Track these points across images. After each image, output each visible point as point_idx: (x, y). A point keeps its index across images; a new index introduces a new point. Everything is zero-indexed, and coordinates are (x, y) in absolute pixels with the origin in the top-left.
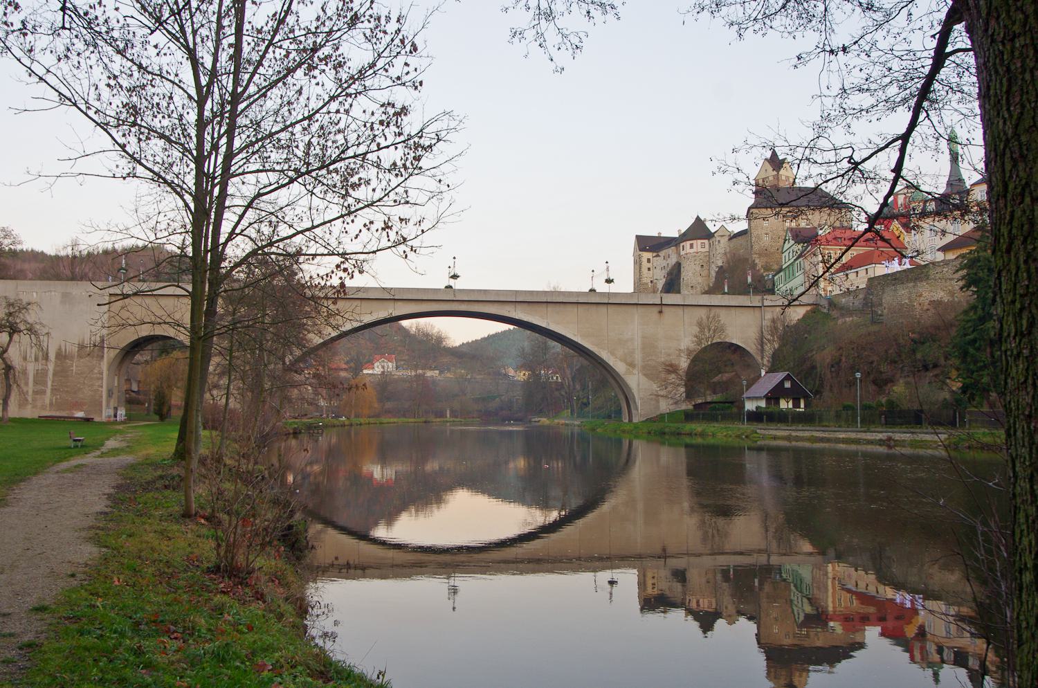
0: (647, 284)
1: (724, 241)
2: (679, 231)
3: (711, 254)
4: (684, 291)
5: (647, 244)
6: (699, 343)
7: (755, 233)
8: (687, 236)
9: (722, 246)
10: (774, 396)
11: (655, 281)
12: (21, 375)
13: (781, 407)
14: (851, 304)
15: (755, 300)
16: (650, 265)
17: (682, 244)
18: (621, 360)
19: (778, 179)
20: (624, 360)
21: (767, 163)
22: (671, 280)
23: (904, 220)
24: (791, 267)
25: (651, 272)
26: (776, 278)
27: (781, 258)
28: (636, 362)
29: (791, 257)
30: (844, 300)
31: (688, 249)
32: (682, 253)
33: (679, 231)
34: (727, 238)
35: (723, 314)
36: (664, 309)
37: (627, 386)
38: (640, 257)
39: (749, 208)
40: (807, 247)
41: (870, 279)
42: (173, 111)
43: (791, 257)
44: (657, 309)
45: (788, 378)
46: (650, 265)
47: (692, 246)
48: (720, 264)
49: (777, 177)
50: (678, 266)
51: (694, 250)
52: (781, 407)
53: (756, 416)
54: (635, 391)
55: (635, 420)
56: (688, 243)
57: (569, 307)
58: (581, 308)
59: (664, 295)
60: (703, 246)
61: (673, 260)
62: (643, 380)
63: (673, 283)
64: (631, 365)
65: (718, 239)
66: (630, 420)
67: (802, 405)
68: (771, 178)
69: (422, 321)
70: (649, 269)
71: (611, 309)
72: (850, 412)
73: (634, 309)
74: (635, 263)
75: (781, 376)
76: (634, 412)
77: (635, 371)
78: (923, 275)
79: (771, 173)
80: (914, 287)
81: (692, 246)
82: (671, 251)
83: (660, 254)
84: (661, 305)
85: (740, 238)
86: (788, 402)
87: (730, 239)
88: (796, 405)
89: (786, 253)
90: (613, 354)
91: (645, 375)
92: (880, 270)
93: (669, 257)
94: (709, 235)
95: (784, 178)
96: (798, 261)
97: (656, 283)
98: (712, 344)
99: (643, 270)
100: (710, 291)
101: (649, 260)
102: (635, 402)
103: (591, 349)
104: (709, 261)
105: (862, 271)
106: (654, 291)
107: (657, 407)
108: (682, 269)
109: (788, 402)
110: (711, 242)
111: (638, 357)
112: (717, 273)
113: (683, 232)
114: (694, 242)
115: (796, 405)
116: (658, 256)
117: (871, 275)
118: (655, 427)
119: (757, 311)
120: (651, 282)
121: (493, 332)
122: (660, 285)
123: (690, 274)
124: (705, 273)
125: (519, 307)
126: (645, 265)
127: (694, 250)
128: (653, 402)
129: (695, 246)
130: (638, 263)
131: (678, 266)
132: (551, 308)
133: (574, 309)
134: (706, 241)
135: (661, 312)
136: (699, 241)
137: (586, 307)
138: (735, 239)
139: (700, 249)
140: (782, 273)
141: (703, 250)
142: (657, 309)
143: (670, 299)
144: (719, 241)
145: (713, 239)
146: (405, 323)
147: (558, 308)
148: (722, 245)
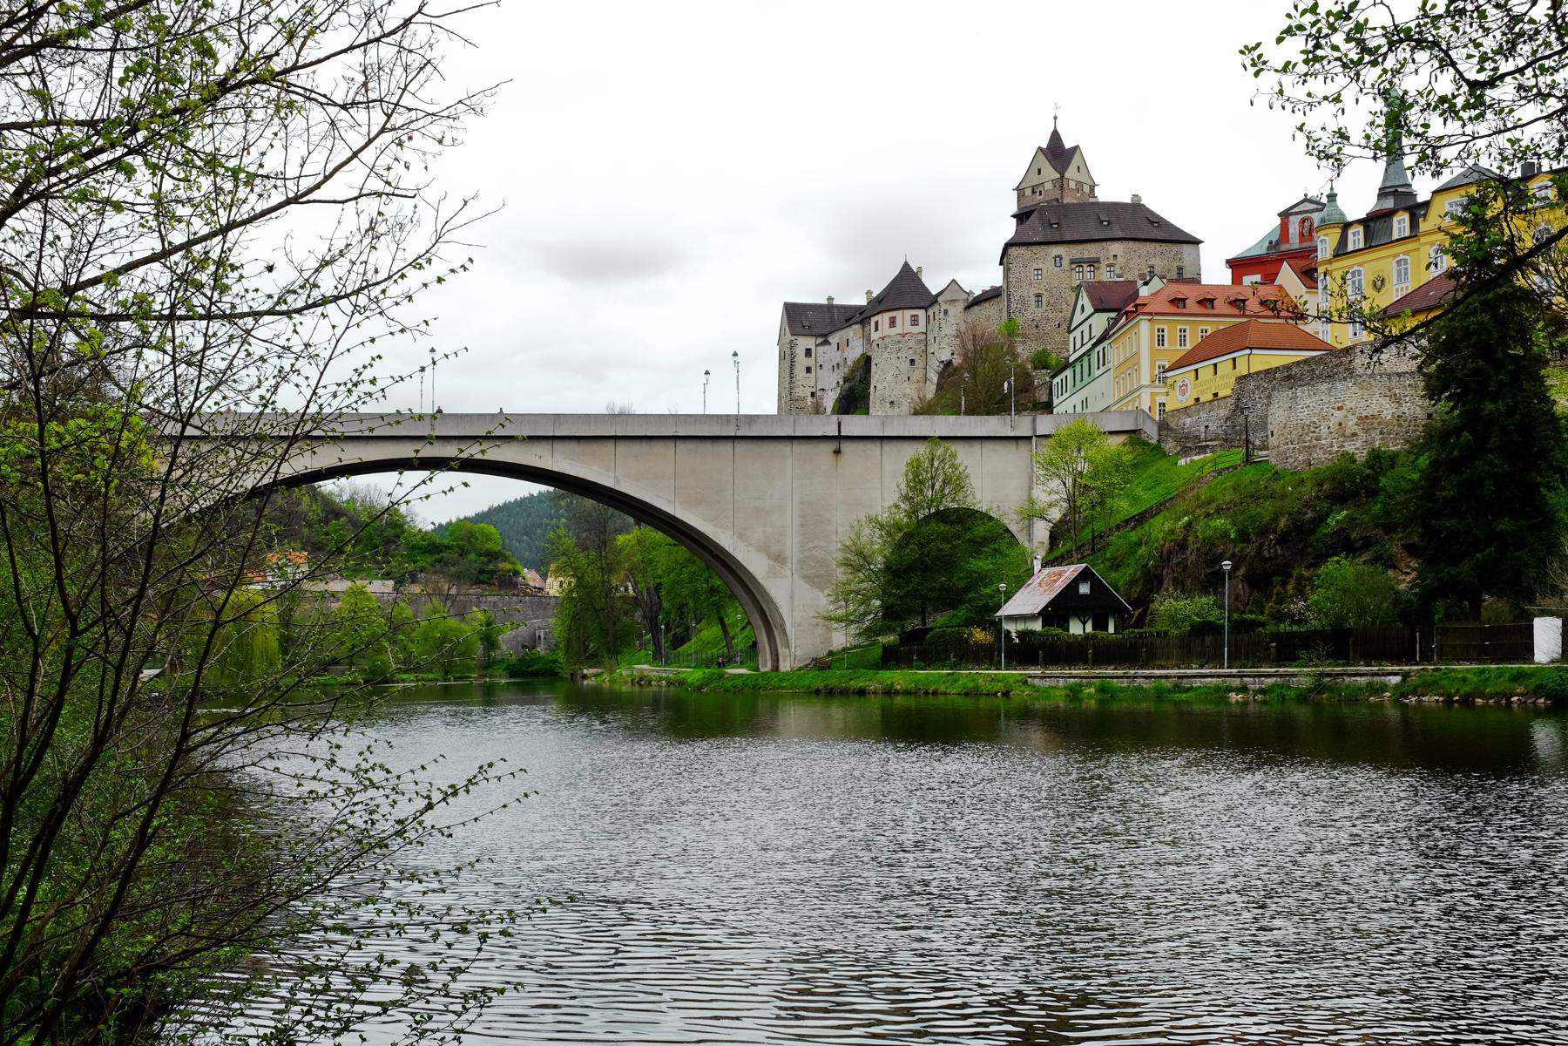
0: (804, 399)
1: (956, 311)
2: (869, 293)
3: (930, 337)
4: (875, 408)
5: (800, 319)
6: (913, 512)
7: (1016, 294)
8: (886, 302)
9: (952, 321)
10: (1057, 612)
11: (819, 393)
12: (877, 401)
13: (1071, 632)
14: (1203, 429)
15: (1022, 425)
16: (810, 362)
17: (873, 320)
18: (759, 549)
19: (1062, 187)
20: (764, 549)
21: (1042, 157)
22: (851, 389)
23: (1302, 263)
24: (1086, 359)
25: (812, 375)
26: (1055, 382)
27: (1066, 343)
28: (788, 554)
29: (1086, 339)
30: (1188, 421)
31: (884, 329)
32: (875, 336)
33: (869, 293)
34: (961, 306)
35: (966, 457)
36: (847, 447)
37: (770, 601)
38: (792, 345)
39: (1008, 246)
40: (1116, 320)
41: (1241, 379)
42: (1512, 142)
43: (1086, 339)
44: (832, 446)
45: (1085, 575)
46: (810, 362)
47: (893, 322)
48: (945, 356)
49: (1061, 183)
50: (866, 361)
51: (898, 329)
52: (1071, 632)
53: (1027, 651)
54: (784, 611)
55: (785, 666)
56: (887, 316)
57: (659, 447)
58: (682, 447)
59: (846, 419)
60: (915, 320)
61: (855, 352)
62: (803, 588)
63: (854, 398)
64: (779, 558)
65: (944, 307)
66: (776, 668)
67: (1111, 629)
68: (1048, 186)
69: (361, 481)
70: (808, 370)
71: (741, 447)
72: (1208, 639)
73: (785, 448)
74: (782, 357)
75: (1071, 571)
76: (782, 651)
77: (787, 571)
78: (1341, 369)
79: (1050, 173)
80: (1330, 390)
81: (893, 322)
82: (854, 333)
83: (830, 339)
84: (840, 438)
85: (987, 305)
86: (1084, 623)
87: (968, 308)
88: (1100, 625)
89: (1077, 333)
90: (742, 536)
91: (805, 577)
92: (1263, 360)
93: (852, 344)
94: (928, 301)
95: (1072, 185)
96: (1099, 348)
97: (821, 398)
98: (937, 513)
99: (796, 371)
100: (925, 409)
101: (808, 352)
102: (784, 631)
103: (701, 529)
104: (925, 351)
105: (1224, 362)
106: (818, 410)
107: (829, 640)
108: (873, 368)
109: (1084, 623)
110: (930, 312)
111: (792, 545)
112: (941, 375)
113: (874, 295)
114: (898, 314)
115: (1100, 625)
116: (826, 343)
117: (1242, 369)
118: (817, 680)
119: (1023, 446)
120: (813, 395)
121: (498, 501)
122: (829, 401)
123: (890, 378)
124: (917, 374)
125: (560, 447)
126: (802, 361)
127: (898, 329)
128: (820, 631)
129: (899, 322)
130: (787, 359)
131: (866, 361)
132: (622, 447)
133: (665, 450)
134: (921, 313)
135: (837, 452)
136: (908, 313)
137: (692, 445)
138: (976, 308)
139: (909, 329)
140: (1068, 372)
141: (916, 330)
142: (829, 447)
143: (854, 425)
144: (946, 312)
145: (935, 308)
146: (328, 486)
147: (636, 448)
148: (951, 319)
